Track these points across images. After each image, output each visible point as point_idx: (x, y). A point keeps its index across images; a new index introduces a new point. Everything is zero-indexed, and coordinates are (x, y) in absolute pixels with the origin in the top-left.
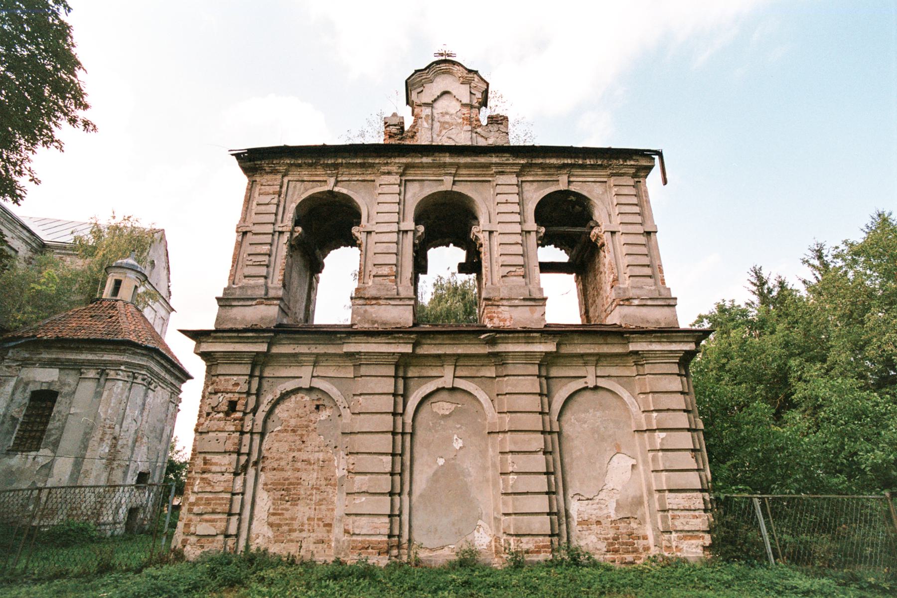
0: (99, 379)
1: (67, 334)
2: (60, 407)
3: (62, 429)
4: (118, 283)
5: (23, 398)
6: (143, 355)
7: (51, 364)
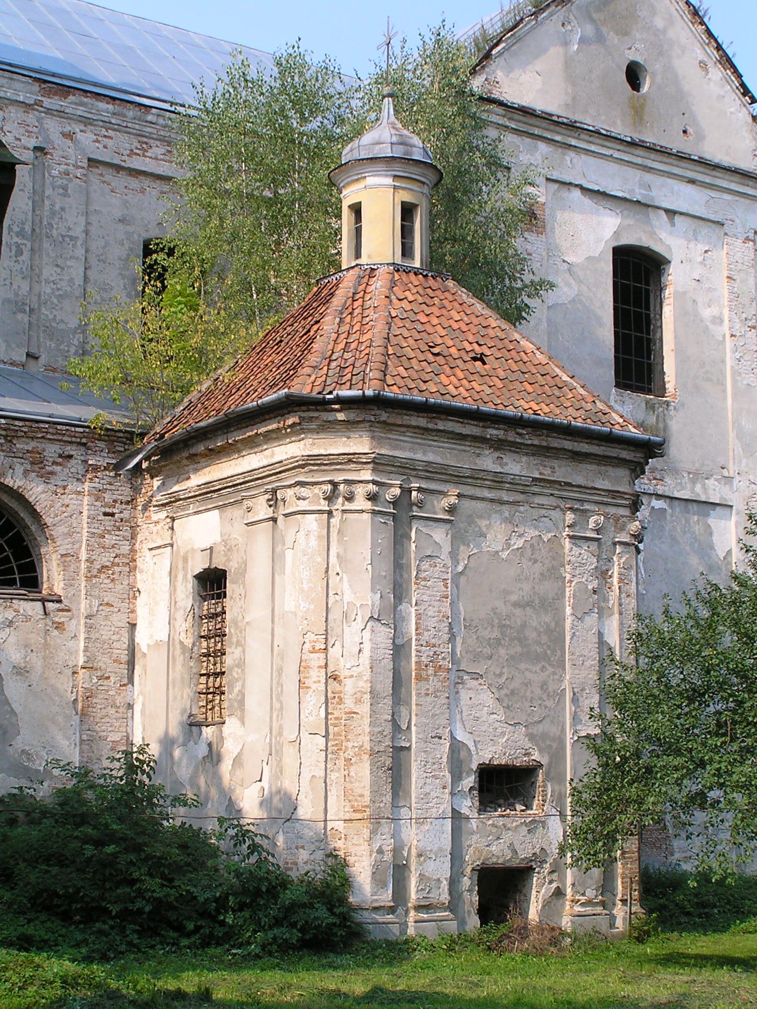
1: (235, 404)
2: (232, 605)
3: (241, 664)
4: (357, 209)
5: (187, 590)
6: (349, 425)
7: (208, 494)
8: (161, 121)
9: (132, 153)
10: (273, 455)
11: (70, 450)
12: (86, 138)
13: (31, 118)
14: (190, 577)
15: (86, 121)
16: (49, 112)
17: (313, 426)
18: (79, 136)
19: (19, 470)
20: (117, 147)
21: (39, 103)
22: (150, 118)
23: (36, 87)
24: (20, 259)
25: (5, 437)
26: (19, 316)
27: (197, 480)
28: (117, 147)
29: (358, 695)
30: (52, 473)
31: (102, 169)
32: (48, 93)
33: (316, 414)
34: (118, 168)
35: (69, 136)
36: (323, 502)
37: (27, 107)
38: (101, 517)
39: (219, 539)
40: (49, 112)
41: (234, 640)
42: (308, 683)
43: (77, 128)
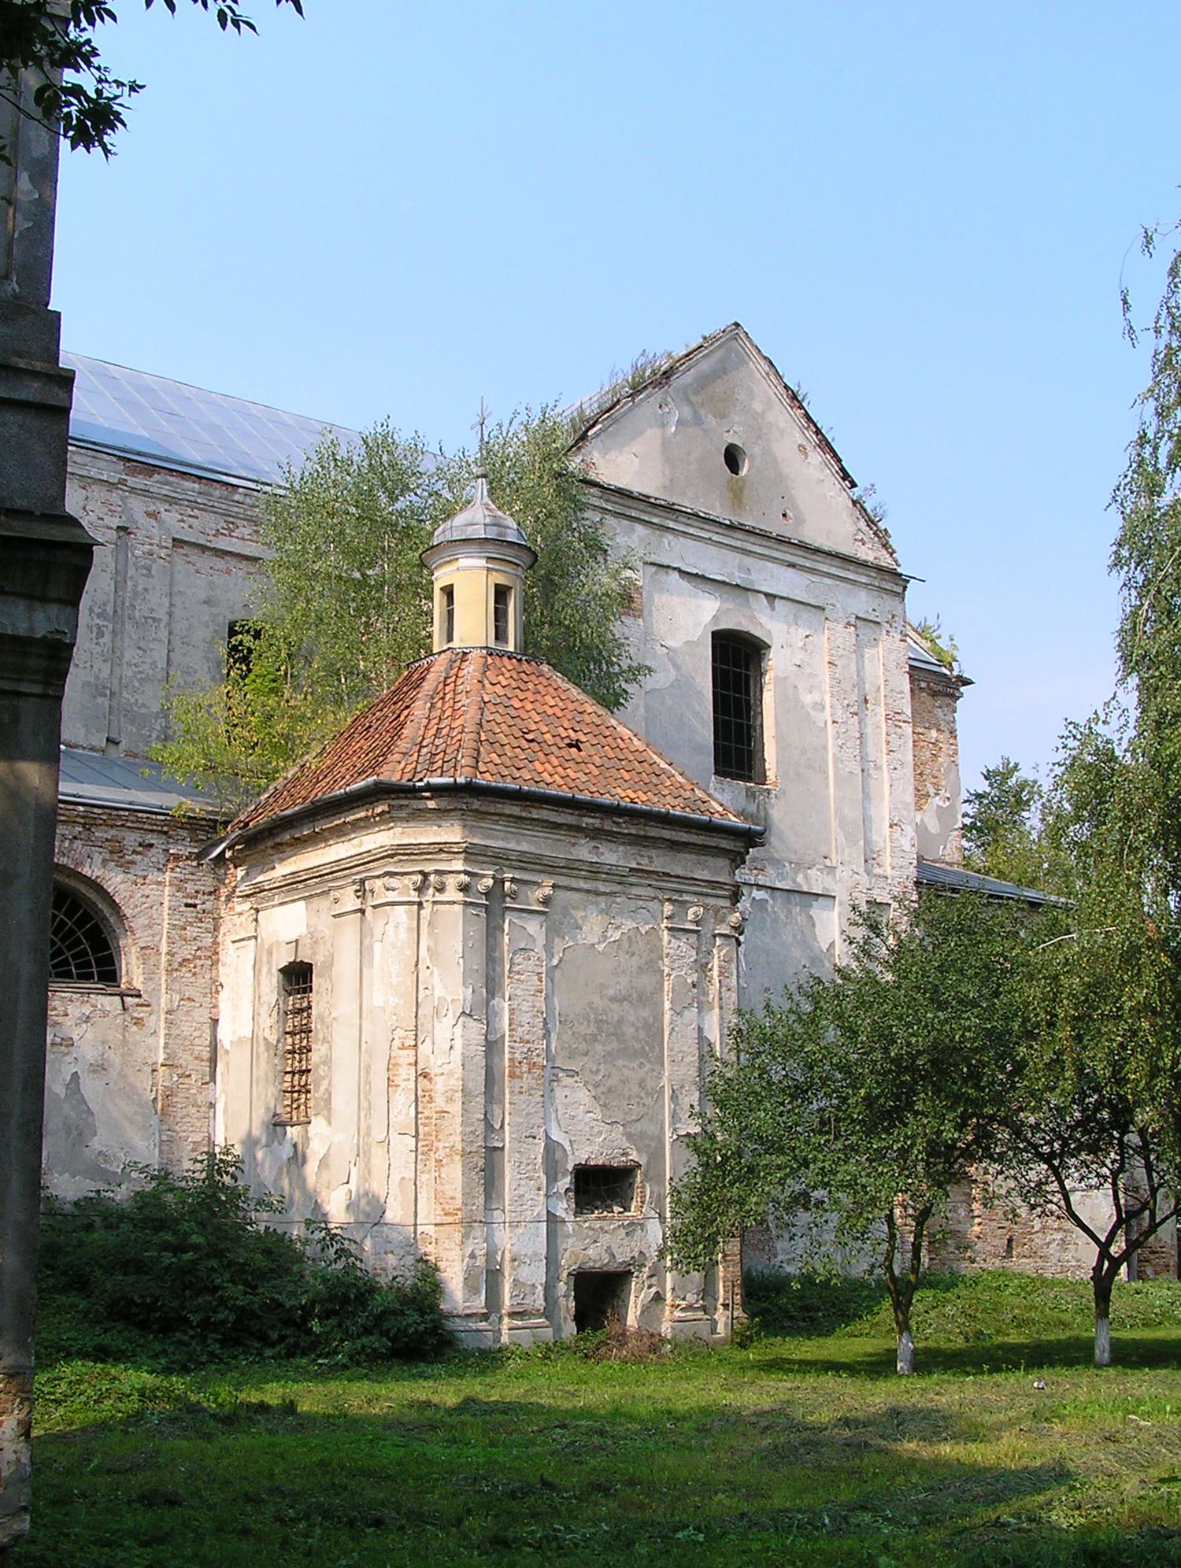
0: (362, 911)
2: (319, 999)
3: (327, 1061)
4: (449, 591)
5: (271, 983)
8: (248, 501)
9: (218, 533)
10: (361, 844)
11: (150, 838)
12: (171, 517)
13: (115, 497)
14: (275, 971)
15: (172, 501)
16: (133, 490)
17: (403, 814)
18: (164, 515)
19: (98, 859)
20: (202, 526)
21: (123, 482)
22: (237, 497)
23: (120, 466)
24: (102, 641)
25: (83, 825)
26: (100, 700)
27: (282, 870)
28: (202, 526)
29: (449, 1094)
30: (133, 862)
31: (186, 550)
32: (133, 472)
33: (406, 802)
34: (203, 548)
35: (153, 515)
36: (413, 893)
37: (111, 485)
38: (183, 909)
39: (304, 931)
40: (133, 490)
41: (321, 1036)
42: (398, 1080)
43: (162, 507)
